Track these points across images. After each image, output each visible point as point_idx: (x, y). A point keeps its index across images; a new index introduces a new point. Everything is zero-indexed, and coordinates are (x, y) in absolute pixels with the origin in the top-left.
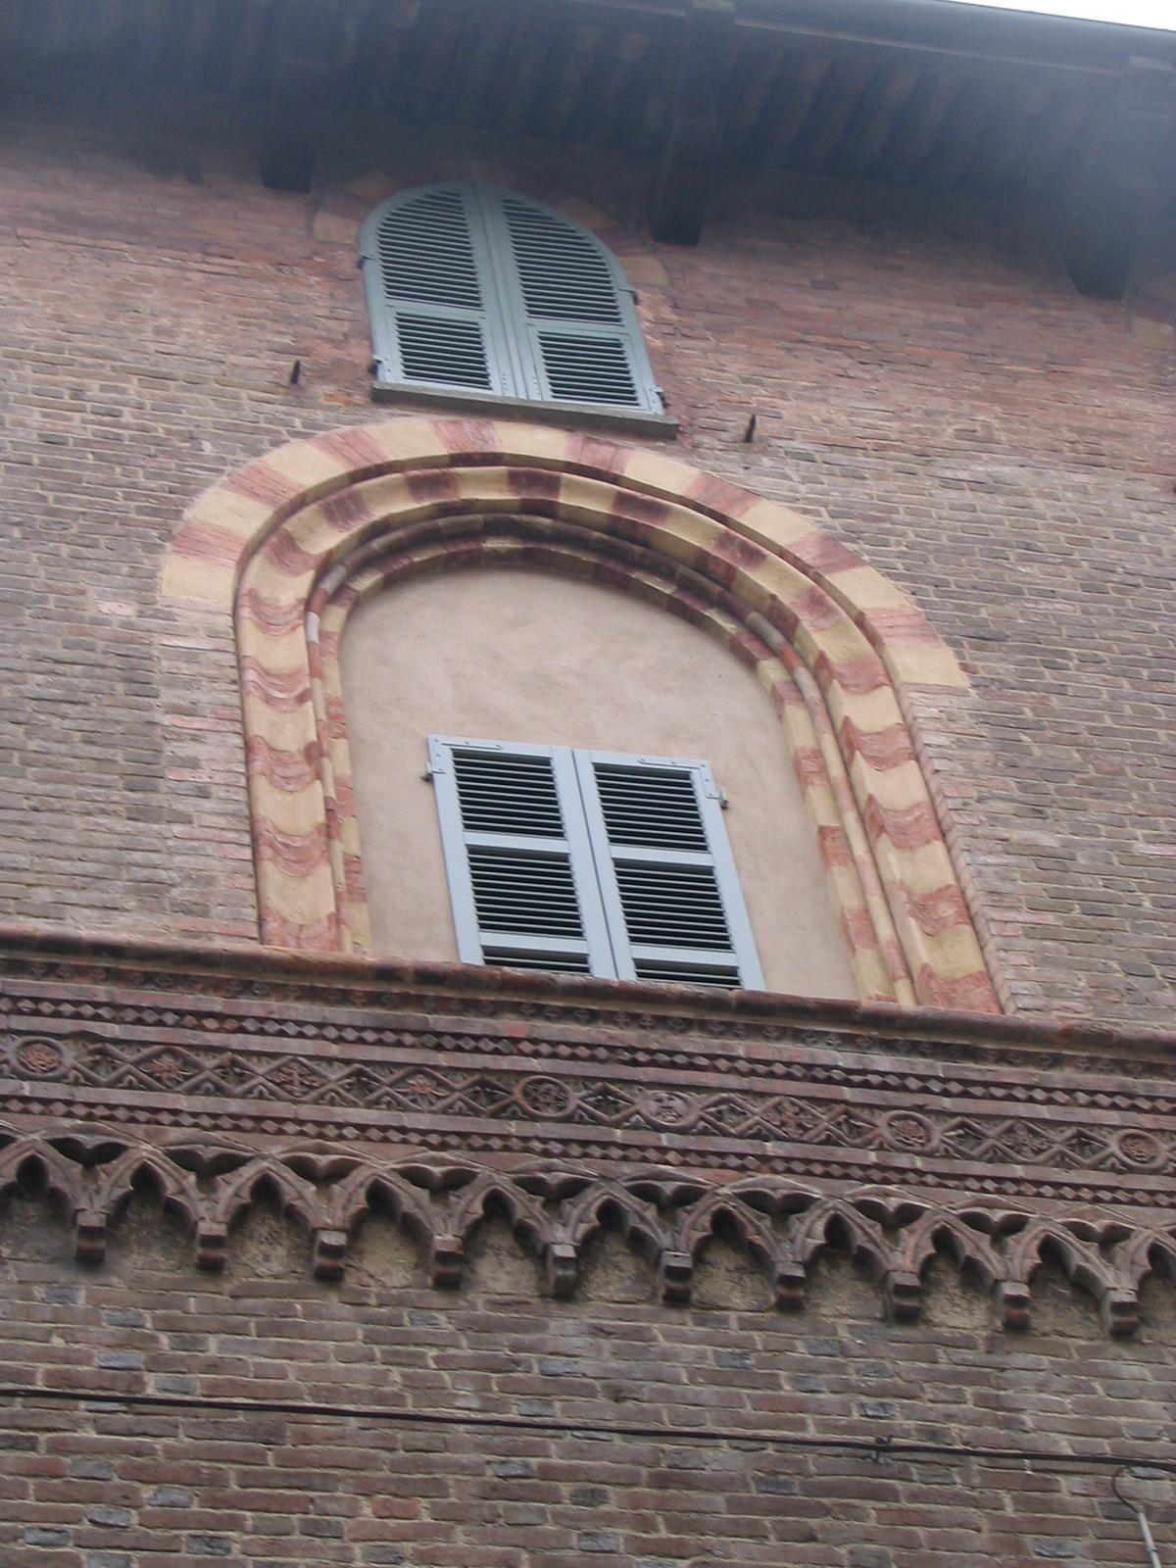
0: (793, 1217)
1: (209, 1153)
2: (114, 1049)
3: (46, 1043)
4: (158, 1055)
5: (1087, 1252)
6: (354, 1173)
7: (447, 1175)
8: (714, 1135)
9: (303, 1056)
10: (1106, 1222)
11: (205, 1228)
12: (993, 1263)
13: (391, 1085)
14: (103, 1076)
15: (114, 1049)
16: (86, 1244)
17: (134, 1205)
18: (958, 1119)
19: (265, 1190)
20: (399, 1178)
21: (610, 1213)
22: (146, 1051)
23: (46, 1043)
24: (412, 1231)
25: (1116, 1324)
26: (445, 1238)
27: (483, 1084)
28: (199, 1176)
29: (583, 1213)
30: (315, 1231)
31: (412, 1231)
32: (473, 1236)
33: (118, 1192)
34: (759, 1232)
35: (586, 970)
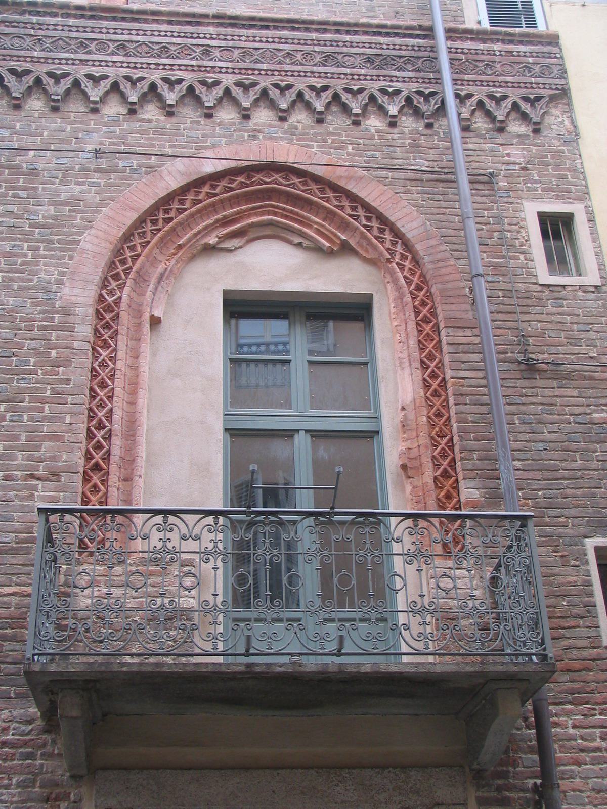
0: (502, 102)
1: (283, 84)
2: (126, 44)
3: (510, 65)
4: (266, 51)
5: (87, 84)
6: (365, 92)
7: (213, 82)
8: (258, 63)
9: (66, 37)
10: (358, 87)
11: (390, 113)
12: (424, 108)
13: (133, 49)
14: (288, 61)
15: (126, 44)
16: (318, 117)
17: (477, 110)
18: (407, 58)
19: (265, 93)
20: (123, 79)
21: (300, 95)
22: (54, 39)
23: (510, 65)
24: (308, 106)
25: (498, 127)
26: (356, 110)
27: (82, 42)
28: (460, 100)
29: (291, 95)
30: (51, 95)
31: (308, 106)
32: (143, 98)
33: (327, 100)
34: (491, 106)
35: (536, 27)
